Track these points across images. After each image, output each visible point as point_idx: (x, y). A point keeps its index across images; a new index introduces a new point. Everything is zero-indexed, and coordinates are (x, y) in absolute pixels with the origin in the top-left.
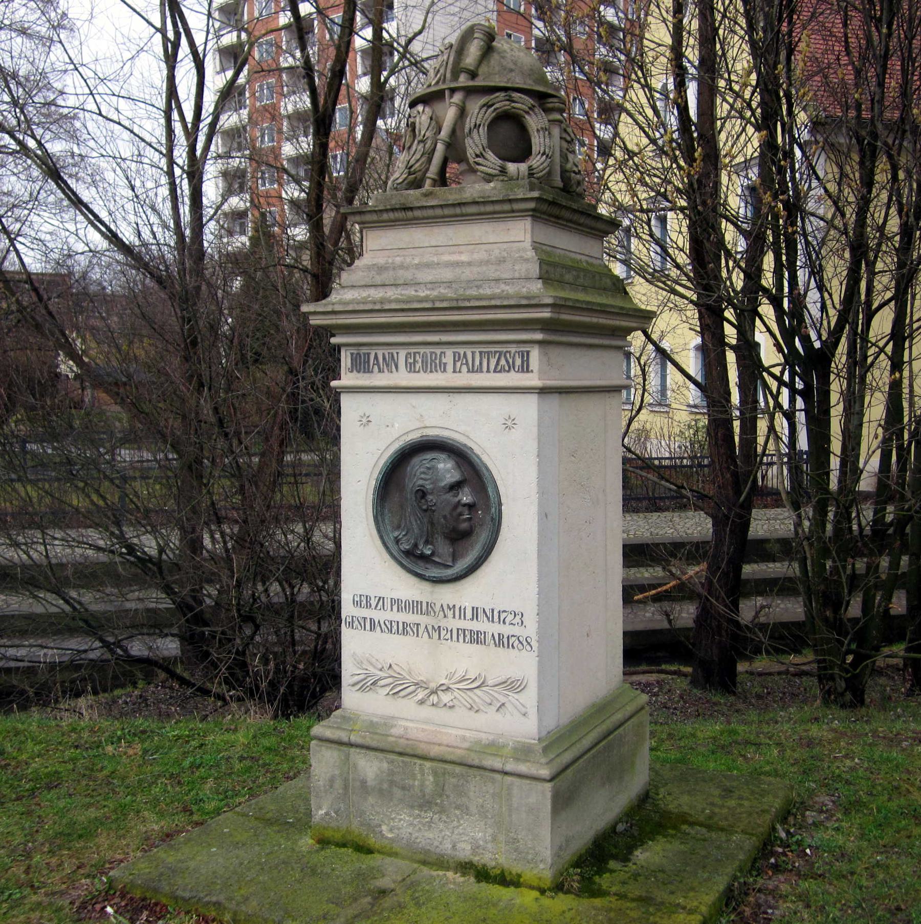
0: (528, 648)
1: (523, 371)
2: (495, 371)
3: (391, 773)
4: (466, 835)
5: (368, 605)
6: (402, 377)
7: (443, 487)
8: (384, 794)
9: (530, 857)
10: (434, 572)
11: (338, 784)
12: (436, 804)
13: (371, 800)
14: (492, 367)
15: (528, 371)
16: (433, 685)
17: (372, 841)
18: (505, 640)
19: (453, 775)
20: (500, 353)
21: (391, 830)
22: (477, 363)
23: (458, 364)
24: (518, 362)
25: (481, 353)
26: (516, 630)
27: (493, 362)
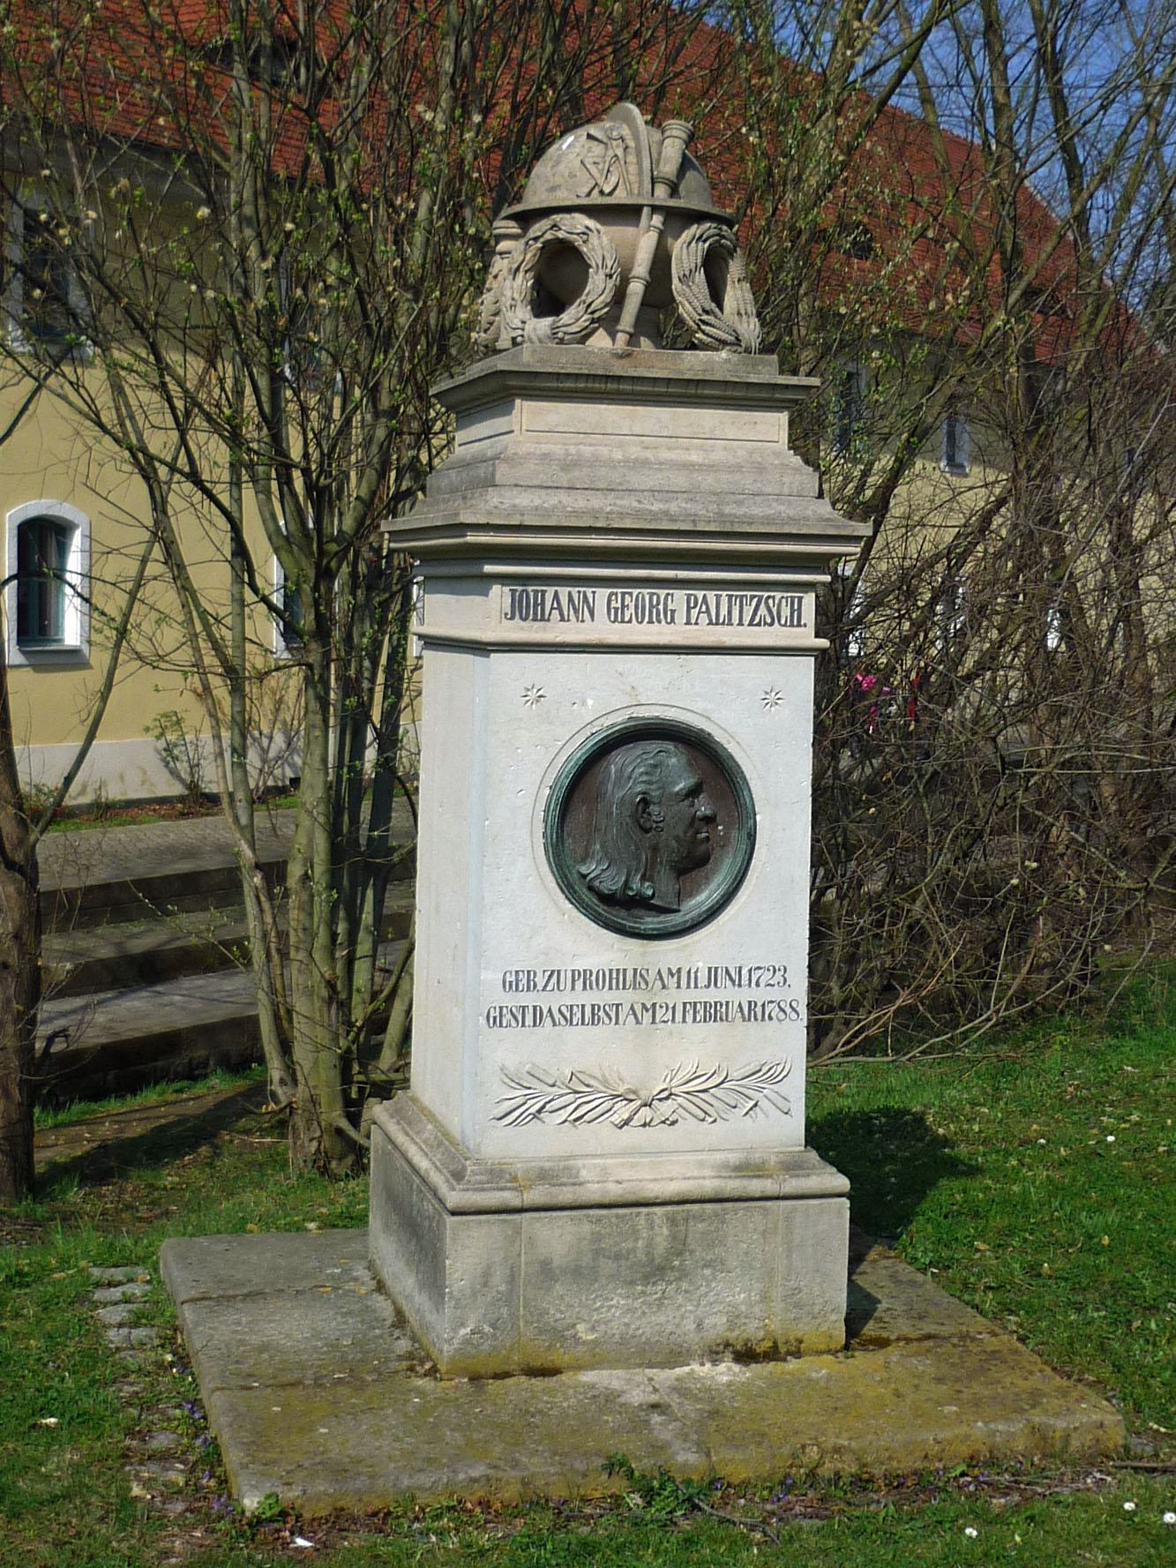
0: (794, 1016)
1: (792, 625)
2: (750, 624)
3: (597, 1238)
4: (726, 1300)
5: (531, 986)
6: (601, 629)
7: (677, 794)
8: (580, 1274)
9: (816, 1309)
10: (651, 922)
11: (499, 1281)
12: (672, 1268)
13: (559, 1288)
14: (747, 620)
15: (799, 625)
16: (644, 1094)
17: (558, 1357)
18: (759, 1010)
19: (700, 1218)
20: (760, 598)
21: (593, 1329)
22: (724, 611)
23: (694, 613)
24: (786, 611)
25: (730, 597)
26: (775, 994)
27: (748, 612)
